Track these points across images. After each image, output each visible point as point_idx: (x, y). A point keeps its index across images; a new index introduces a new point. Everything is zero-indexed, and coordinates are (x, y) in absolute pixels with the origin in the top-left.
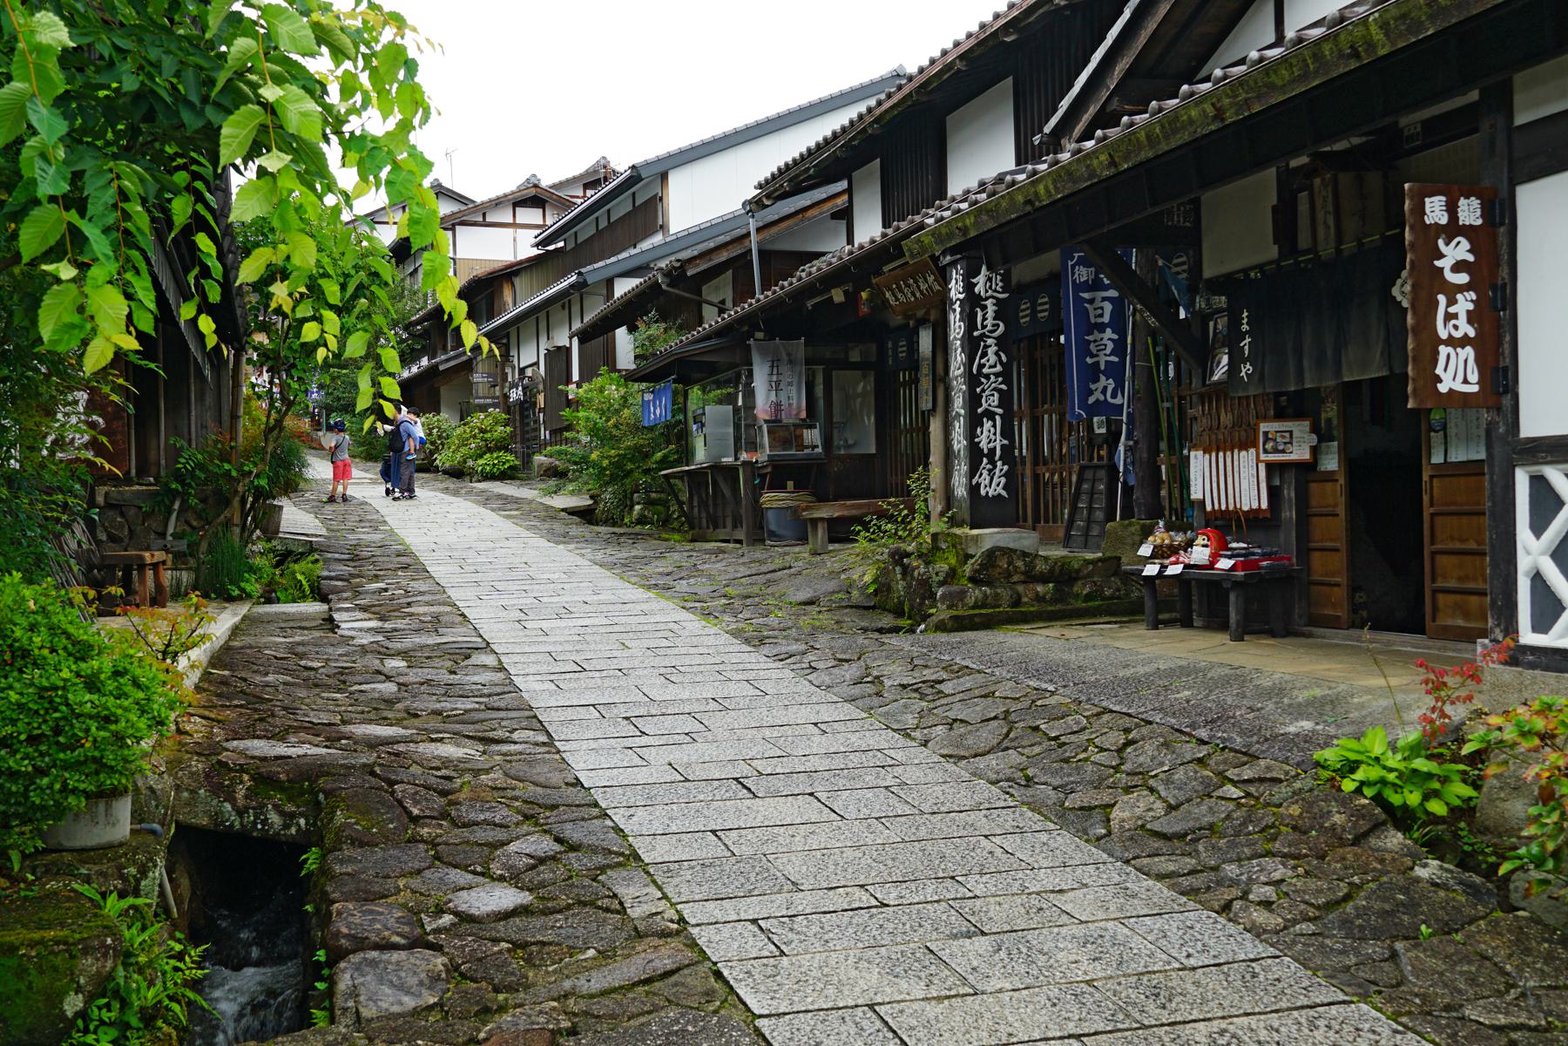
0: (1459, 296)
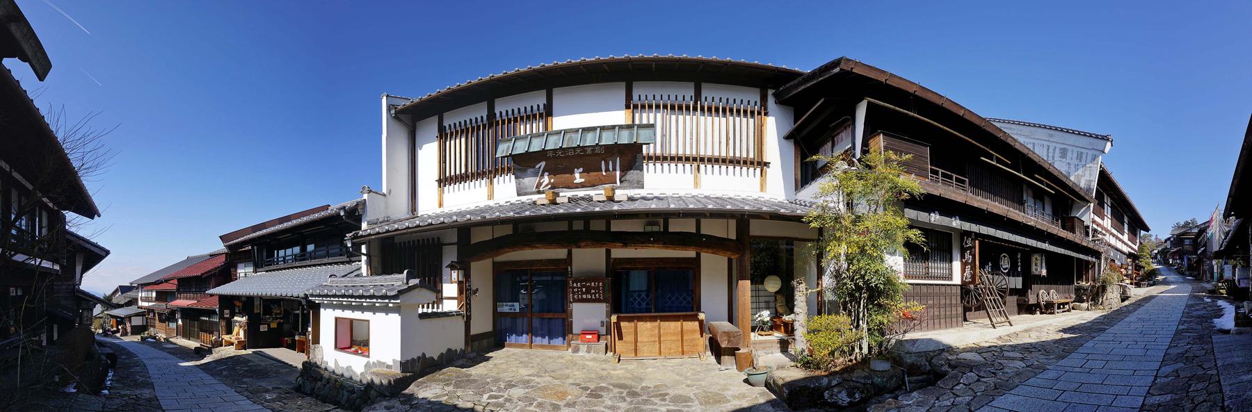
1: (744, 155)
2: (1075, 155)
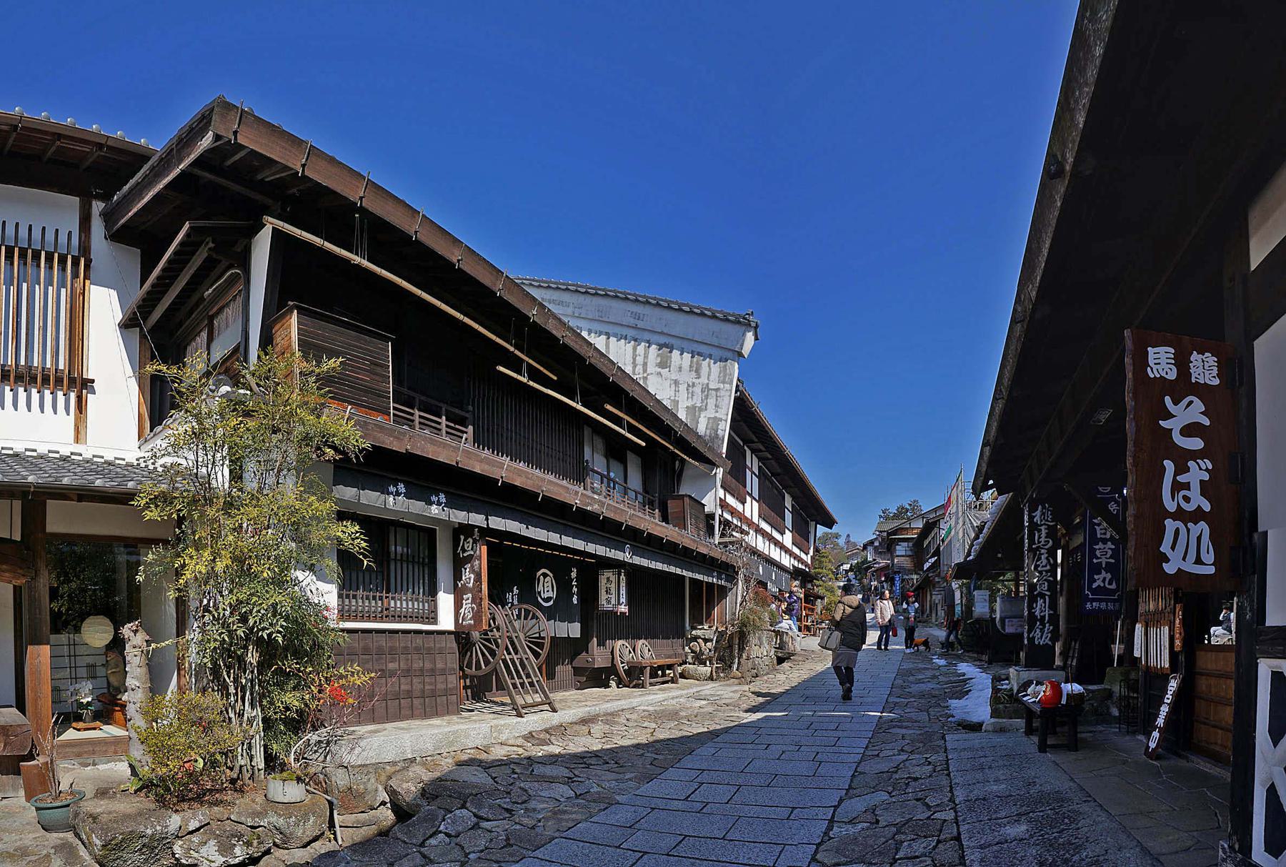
0: (1191, 464)
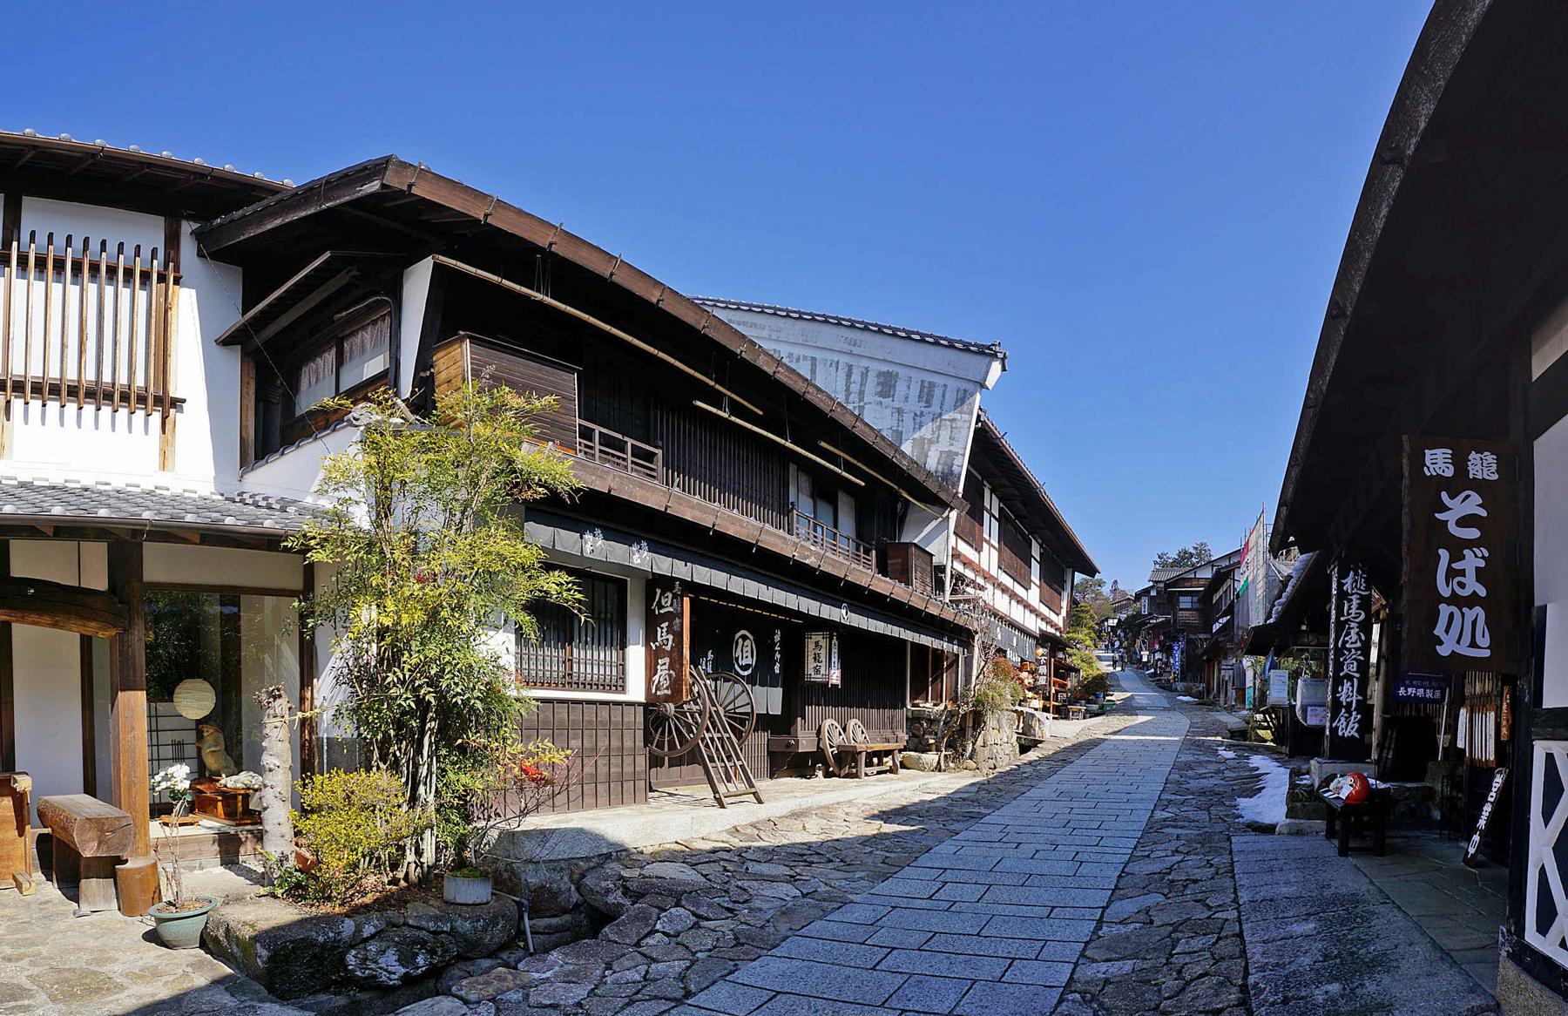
0: (1466, 552)
1: (123, 379)
2: (915, 390)
